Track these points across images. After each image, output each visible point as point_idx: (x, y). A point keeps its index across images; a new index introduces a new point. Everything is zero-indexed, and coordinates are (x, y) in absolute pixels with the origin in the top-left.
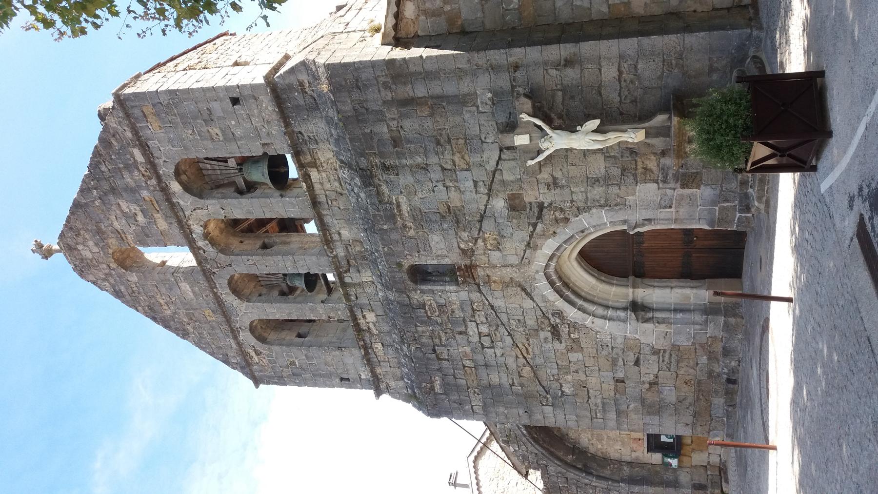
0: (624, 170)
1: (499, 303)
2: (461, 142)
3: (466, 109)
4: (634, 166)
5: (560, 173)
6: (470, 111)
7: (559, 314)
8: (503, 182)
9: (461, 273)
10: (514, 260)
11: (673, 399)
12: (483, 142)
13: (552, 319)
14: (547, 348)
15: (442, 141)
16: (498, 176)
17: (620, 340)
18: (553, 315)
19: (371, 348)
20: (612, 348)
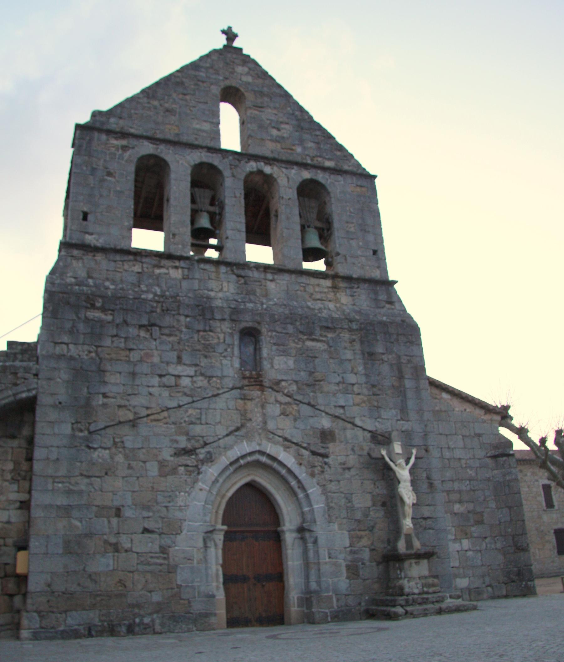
0: (359, 521)
1: (220, 403)
2: (376, 404)
3: (399, 412)
4: (363, 528)
5: (354, 473)
6: (397, 414)
7: (210, 459)
8: (345, 429)
9: (253, 378)
10: (271, 425)
11: (91, 568)
12: (376, 419)
13: (203, 451)
14: (162, 440)
15: (375, 389)
16: (349, 426)
17: (179, 515)
18: (208, 452)
19: (136, 260)
20: (166, 507)
